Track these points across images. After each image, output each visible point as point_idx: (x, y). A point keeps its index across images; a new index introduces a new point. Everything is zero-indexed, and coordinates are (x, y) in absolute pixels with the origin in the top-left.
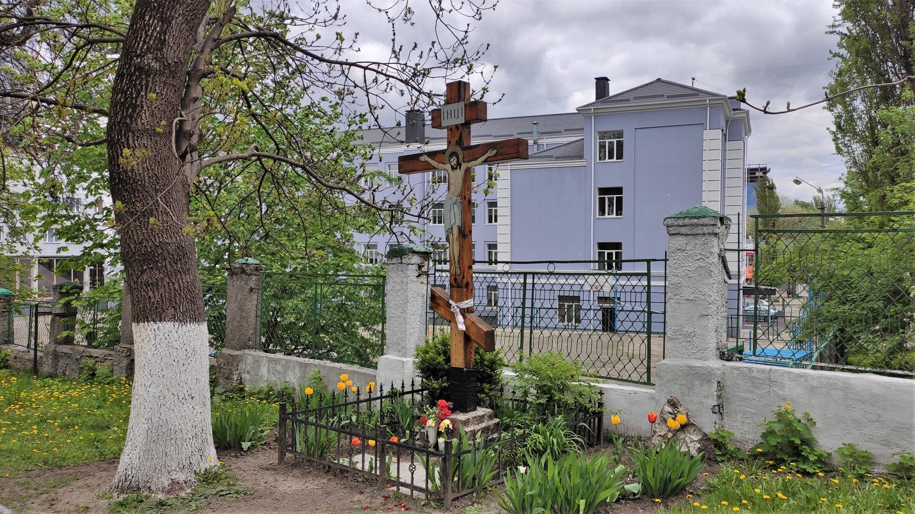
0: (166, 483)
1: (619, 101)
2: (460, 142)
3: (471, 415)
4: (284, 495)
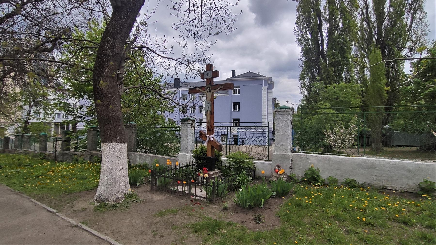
0: (114, 199)
2: (210, 84)
3: (214, 172)
4: (156, 201)
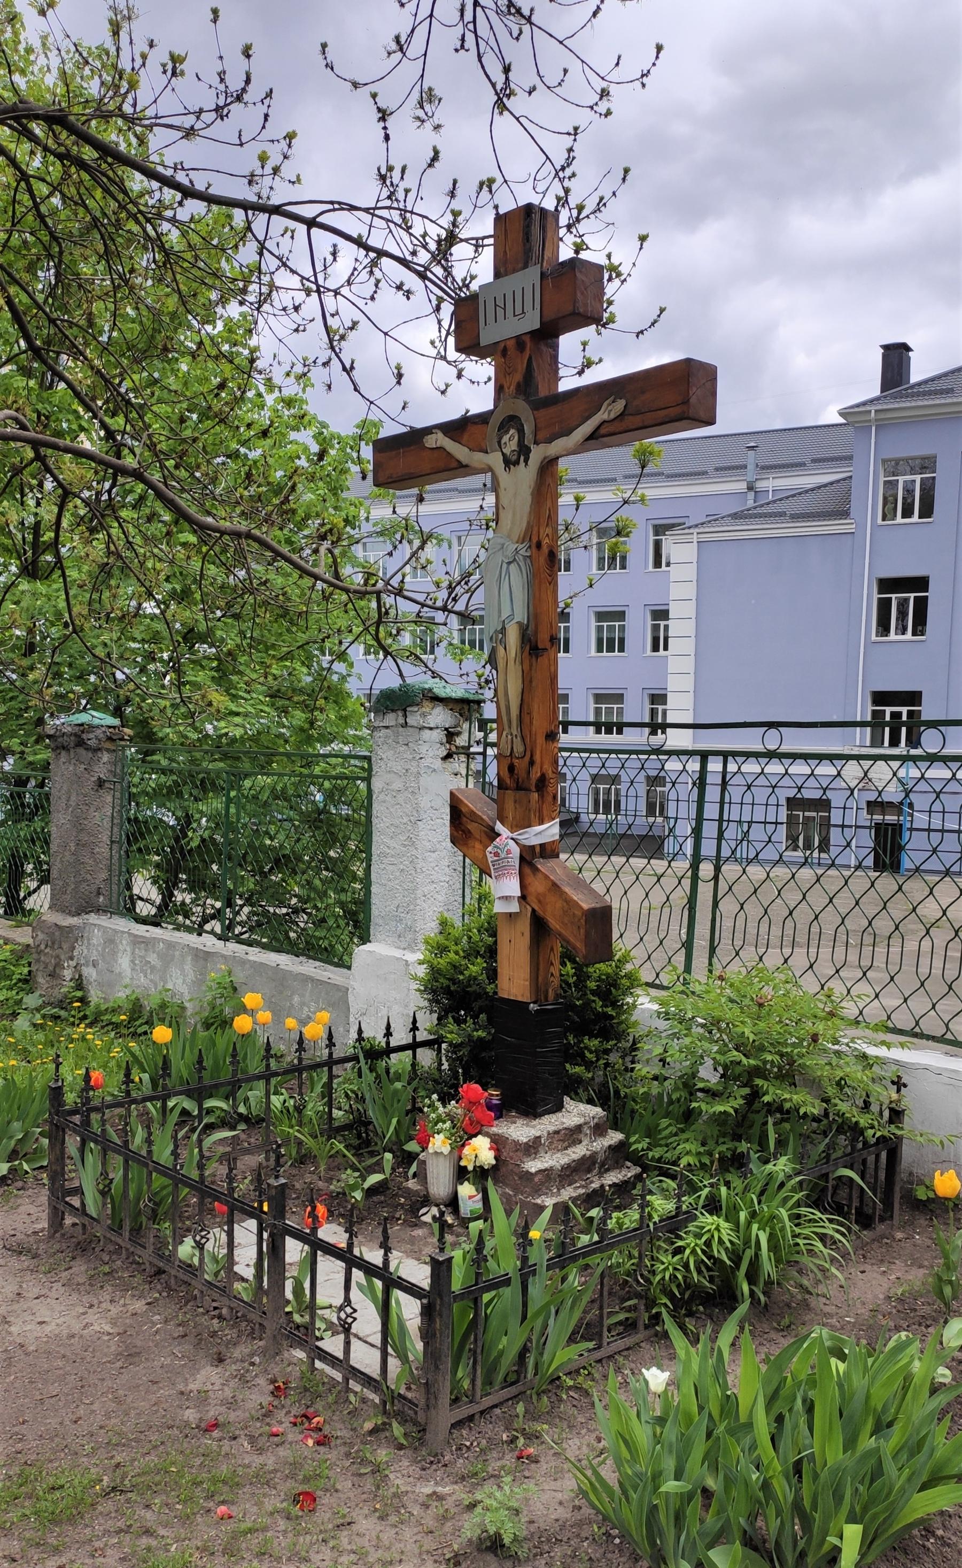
1: (930, 393)
2: (526, 387)
